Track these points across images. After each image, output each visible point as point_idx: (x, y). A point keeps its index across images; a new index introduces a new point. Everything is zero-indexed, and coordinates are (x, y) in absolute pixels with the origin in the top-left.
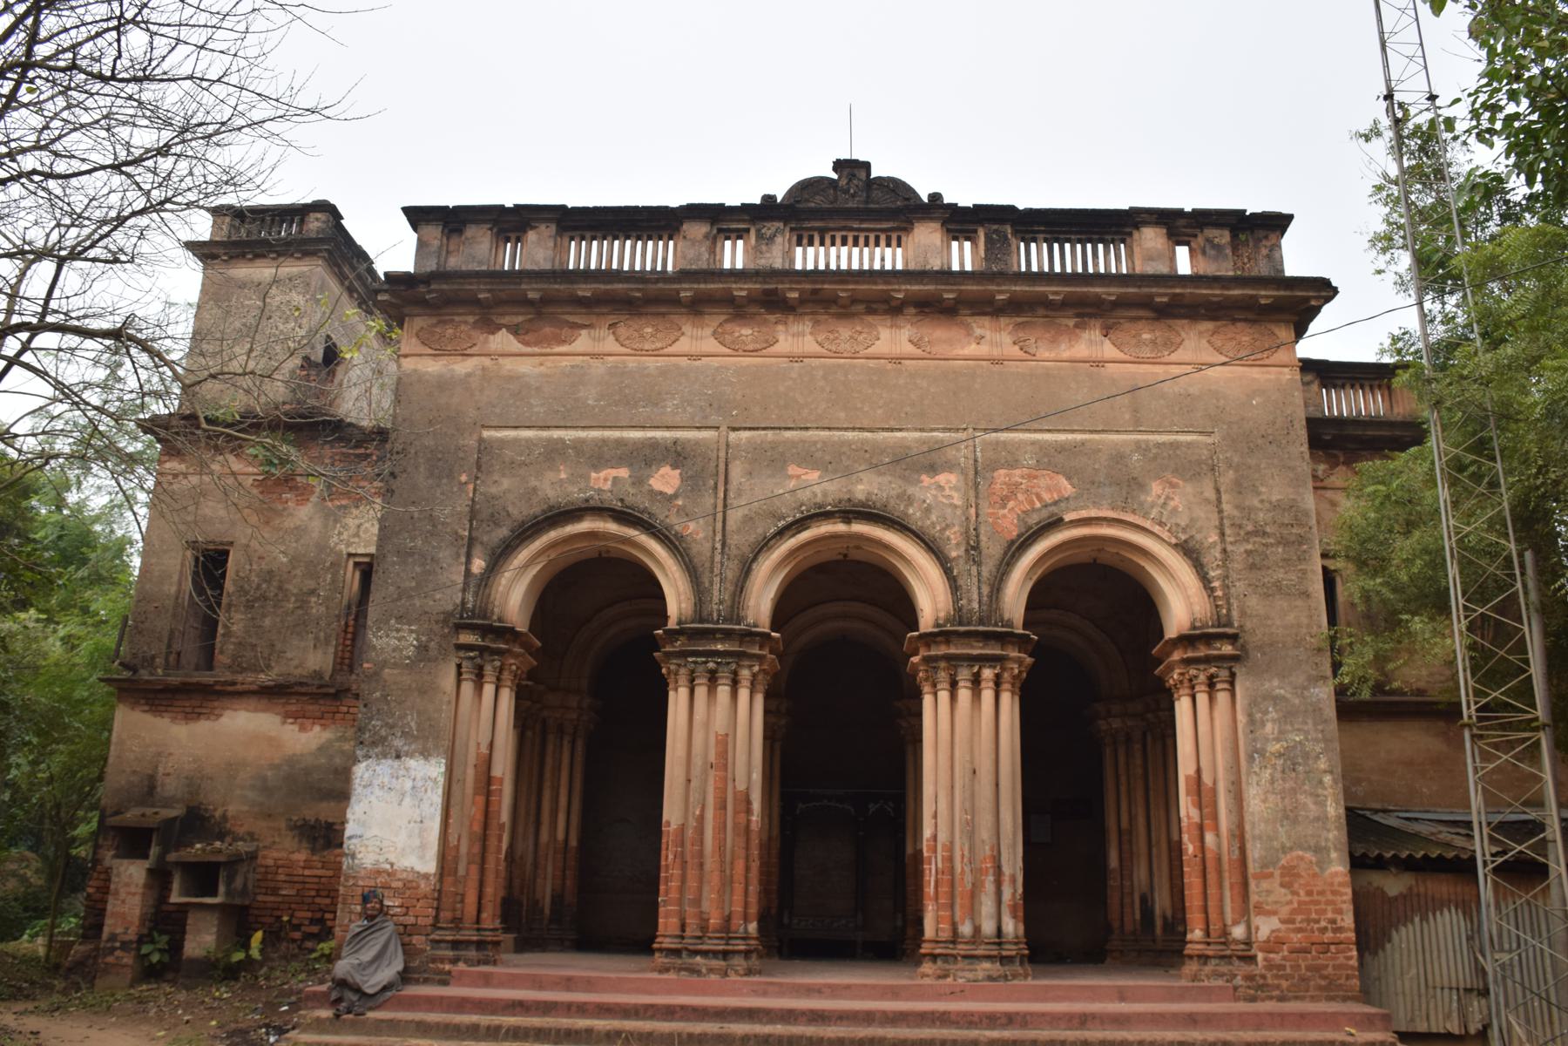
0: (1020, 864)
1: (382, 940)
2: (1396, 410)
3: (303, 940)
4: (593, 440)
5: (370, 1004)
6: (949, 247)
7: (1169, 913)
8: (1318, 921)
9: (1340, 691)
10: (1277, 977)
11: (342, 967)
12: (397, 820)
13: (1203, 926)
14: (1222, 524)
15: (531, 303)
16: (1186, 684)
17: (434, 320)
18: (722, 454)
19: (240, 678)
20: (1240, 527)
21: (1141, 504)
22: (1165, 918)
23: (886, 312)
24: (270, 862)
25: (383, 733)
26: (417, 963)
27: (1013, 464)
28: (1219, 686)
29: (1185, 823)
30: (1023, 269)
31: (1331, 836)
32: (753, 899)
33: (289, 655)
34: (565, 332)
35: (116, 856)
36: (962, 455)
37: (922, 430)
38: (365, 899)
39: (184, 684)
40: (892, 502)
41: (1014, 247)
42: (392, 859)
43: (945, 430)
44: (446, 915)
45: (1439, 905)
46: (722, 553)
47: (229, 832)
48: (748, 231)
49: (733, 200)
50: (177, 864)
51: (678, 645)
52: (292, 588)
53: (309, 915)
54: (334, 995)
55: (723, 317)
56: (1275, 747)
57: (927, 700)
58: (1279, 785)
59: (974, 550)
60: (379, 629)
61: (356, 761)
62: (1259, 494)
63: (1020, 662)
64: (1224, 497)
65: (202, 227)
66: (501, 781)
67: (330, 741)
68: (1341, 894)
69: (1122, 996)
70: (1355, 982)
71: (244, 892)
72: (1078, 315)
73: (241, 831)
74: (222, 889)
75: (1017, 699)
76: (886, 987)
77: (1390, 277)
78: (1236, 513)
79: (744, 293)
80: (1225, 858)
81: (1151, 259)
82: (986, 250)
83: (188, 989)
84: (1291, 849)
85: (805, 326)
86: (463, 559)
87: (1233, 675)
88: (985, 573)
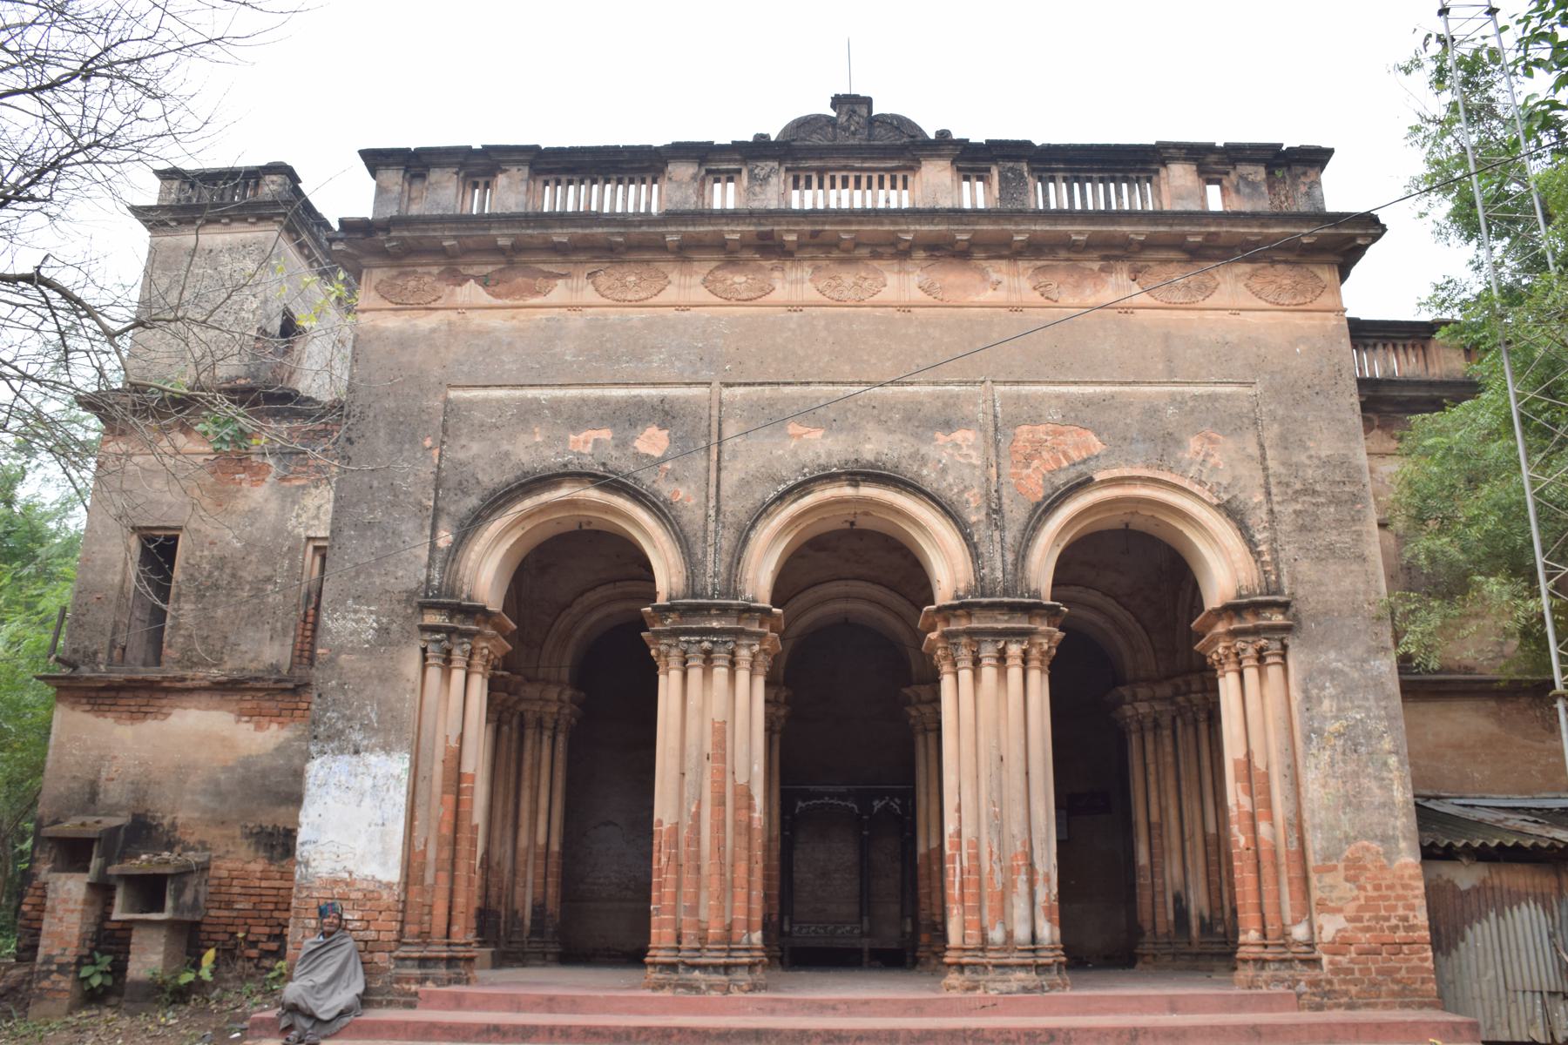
0: (1054, 861)
1: (340, 959)
2: (1431, 371)
3: (260, 958)
4: (572, 399)
5: (326, 1031)
6: (960, 187)
7: (1206, 913)
8: (1387, 919)
9: (1405, 661)
10: (1345, 982)
11: (292, 991)
12: (357, 824)
13: (1258, 926)
14: (1267, 483)
15: (501, 251)
16: (1233, 658)
17: (394, 272)
18: (715, 412)
19: (189, 674)
20: (1288, 485)
21: (1178, 462)
22: (1202, 918)
23: (894, 256)
24: (224, 874)
25: (340, 726)
26: (379, 984)
27: (1036, 420)
28: (1269, 660)
29: (1233, 812)
30: (1041, 207)
31: (1398, 823)
32: (757, 906)
33: (243, 648)
34: (540, 282)
35: (54, 870)
36: (980, 412)
37: (935, 383)
38: (322, 913)
39: (129, 681)
40: (904, 463)
41: (1030, 187)
42: (351, 867)
43: (961, 383)
44: (411, 929)
45: (1516, 898)
46: (717, 520)
47: (178, 842)
48: (739, 172)
49: (723, 138)
50: (120, 877)
51: (670, 622)
52: (246, 575)
53: (267, 930)
54: (284, 1023)
55: (714, 264)
56: (1333, 726)
57: (947, 682)
58: (1340, 768)
59: (995, 513)
60: (335, 610)
61: (308, 757)
62: (1307, 449)
63: (1049, 636)
64: (1269, 453)
65: (150, 192)
66: (473, 777)
67: (288, 740)
68: (1413, 889)
69: (1173, 1006)
70: (1432, 986)
71: (195, 906)
72: (1105, 258)
73: (192, 840)
74: (169, 903)
75: (1046, 677)
76: (910, 1002)
77: (1428, 225)
78: (1282, 470)
79: (737, 236)
80: (1282, 850)
81: (1181, 198)
82: (1001, 190)
83: (133, 1015)
84: (1355, 838)
85: (803, 272)
86: (428, 532)
87: (1285, 647)
88: (1009, 539)
